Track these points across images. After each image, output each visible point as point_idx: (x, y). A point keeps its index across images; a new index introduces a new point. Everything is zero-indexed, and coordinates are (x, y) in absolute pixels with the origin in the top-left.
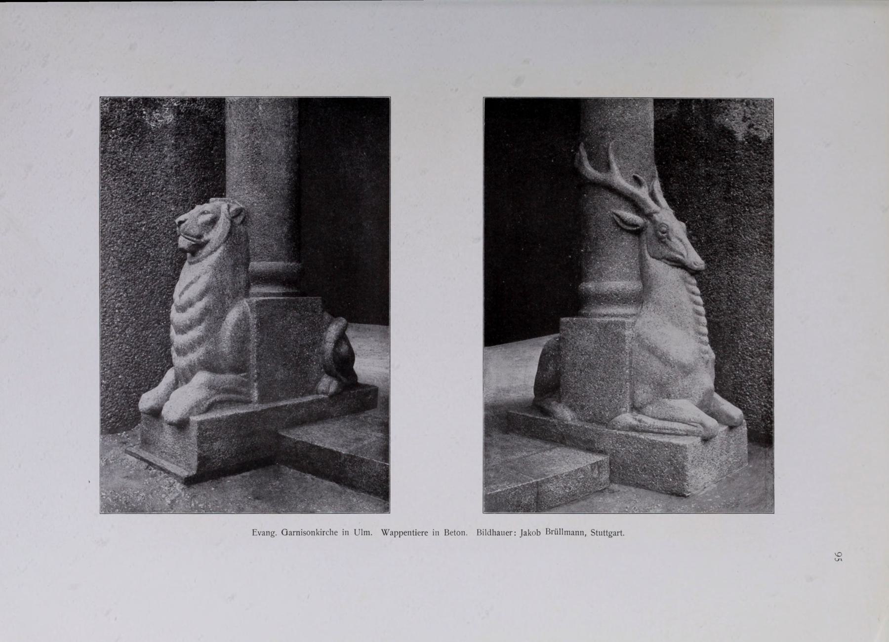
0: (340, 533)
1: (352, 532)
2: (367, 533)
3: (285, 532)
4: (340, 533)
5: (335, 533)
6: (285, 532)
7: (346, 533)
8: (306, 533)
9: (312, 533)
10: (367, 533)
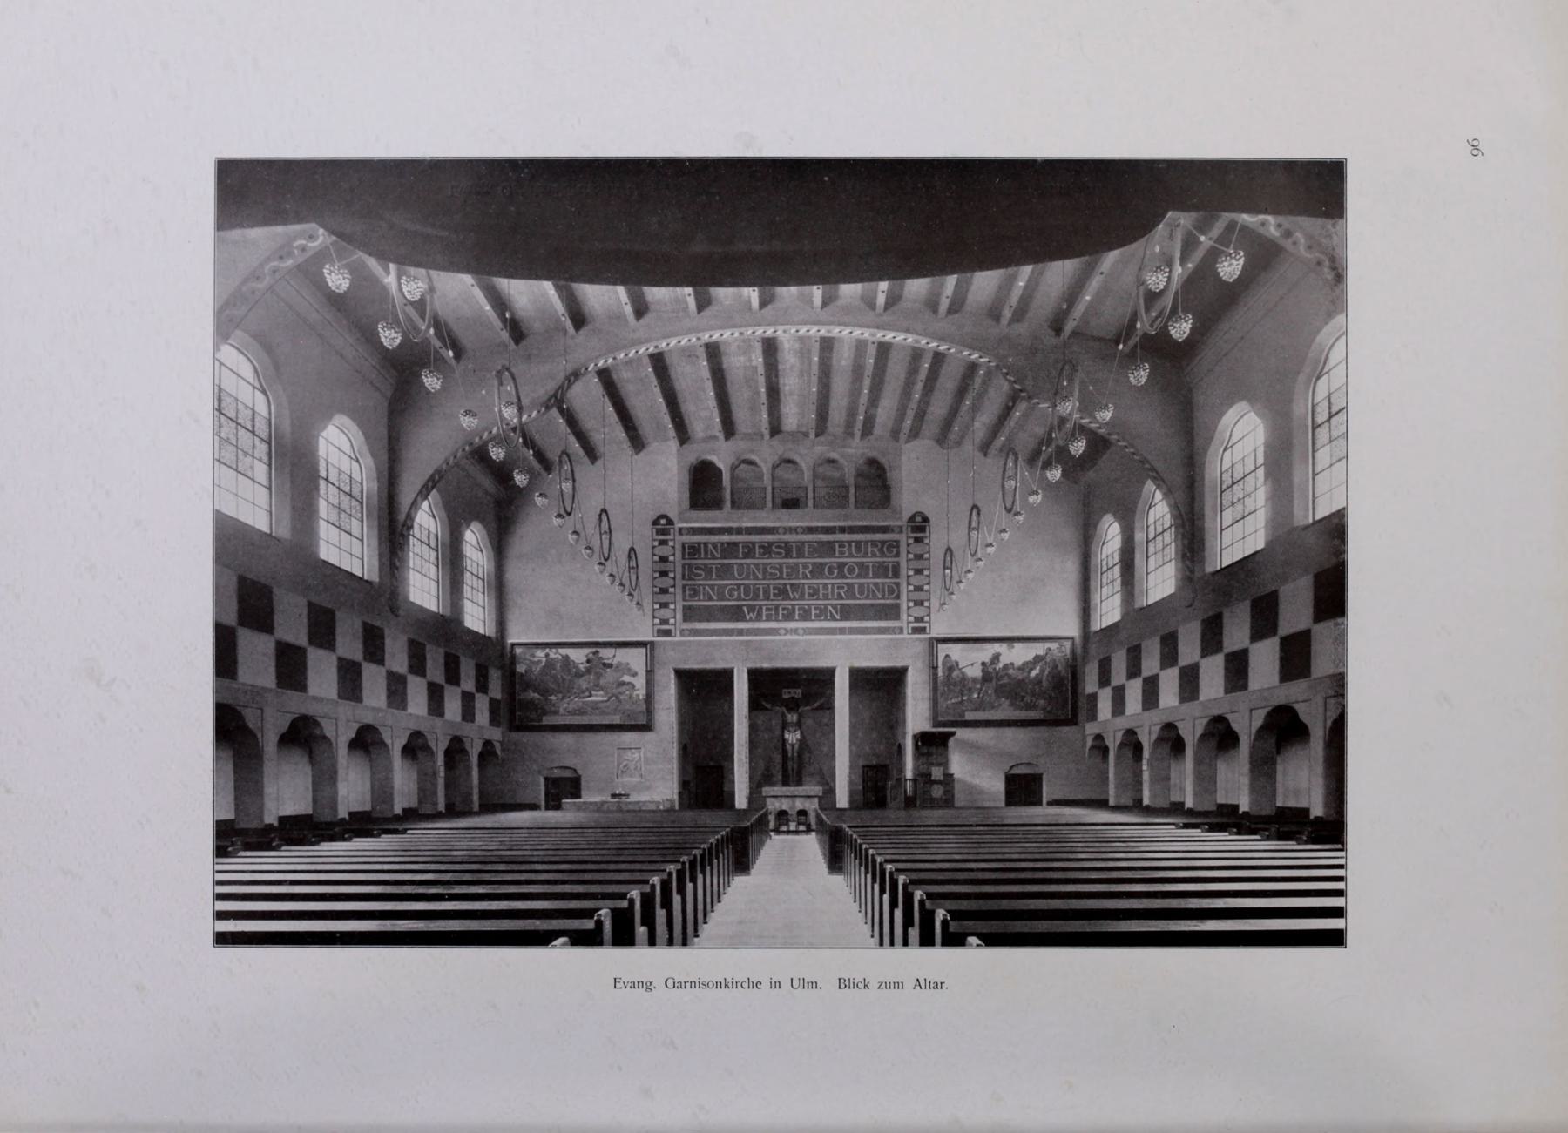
1: (786, 984)
2: (814, 985)
6: (670, 983)
7: (778, 985)
8: (706, 985)
9: (718, 985)
10: (814, 985)
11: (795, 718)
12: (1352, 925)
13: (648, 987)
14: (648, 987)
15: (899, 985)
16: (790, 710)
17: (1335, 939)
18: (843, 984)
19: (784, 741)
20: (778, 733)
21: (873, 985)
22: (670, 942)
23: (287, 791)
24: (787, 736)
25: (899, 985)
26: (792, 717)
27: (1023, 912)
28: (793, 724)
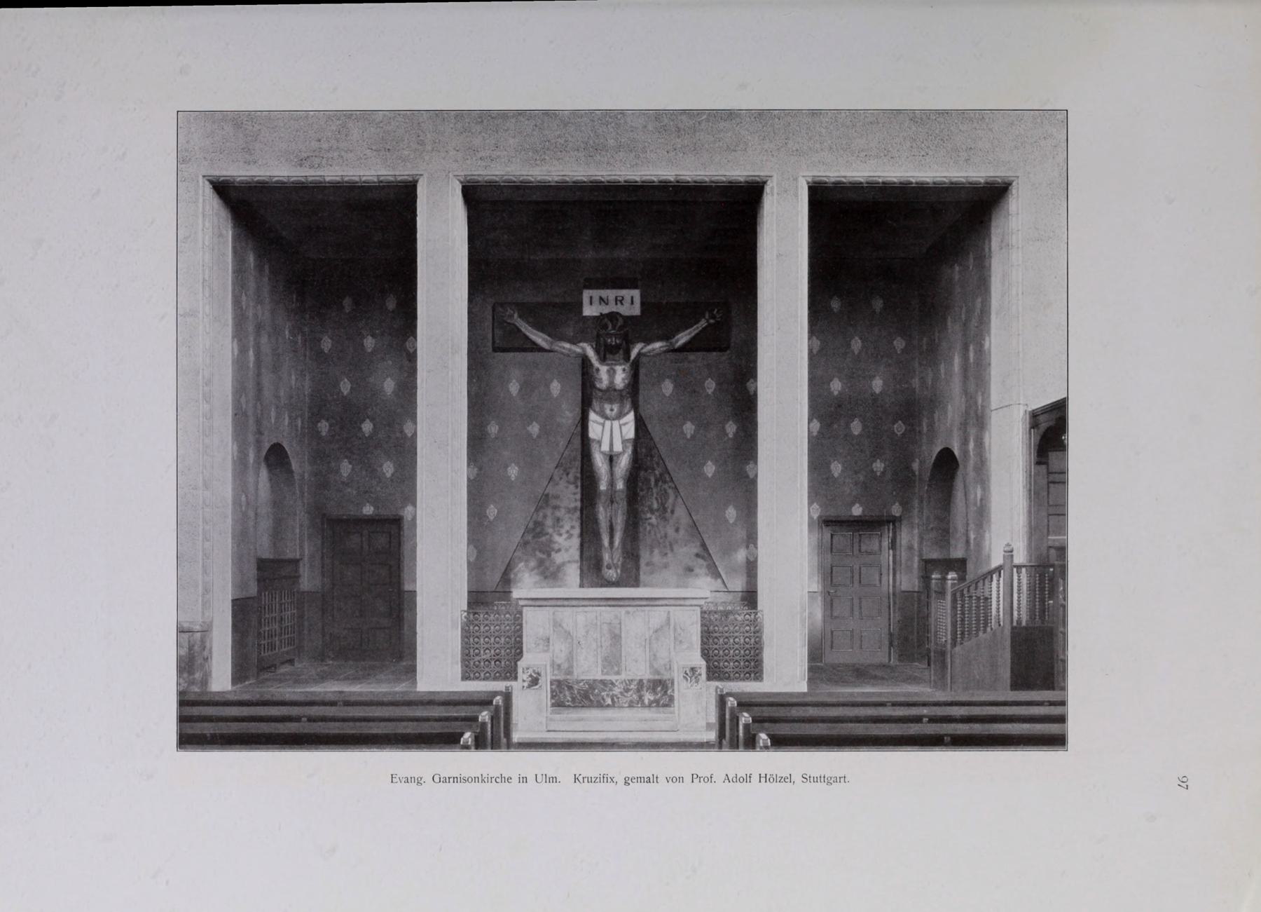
0: (515, 780)
1: (531, 779)
2: (554, 780)
3: (437, 779)
4: (515, 780)
6: (437, 779)
7: (524, 780)
9: (476, 779)
10: (554, 780)
11: (621, 377)
12: (1074, 729)
13: (419, 782)
14: (419, 782)
15: (681, 779)
16: (606, 352)
17: (1058, 741)
19: (585, 443)
20: (568, 415)
21: (797, 778)
22: (1062, 719)
23: (381, 541)
24: (595, 430)
25: (681, 779)
26: (615, 375)
27: (264, 735)
28: (611, 394)
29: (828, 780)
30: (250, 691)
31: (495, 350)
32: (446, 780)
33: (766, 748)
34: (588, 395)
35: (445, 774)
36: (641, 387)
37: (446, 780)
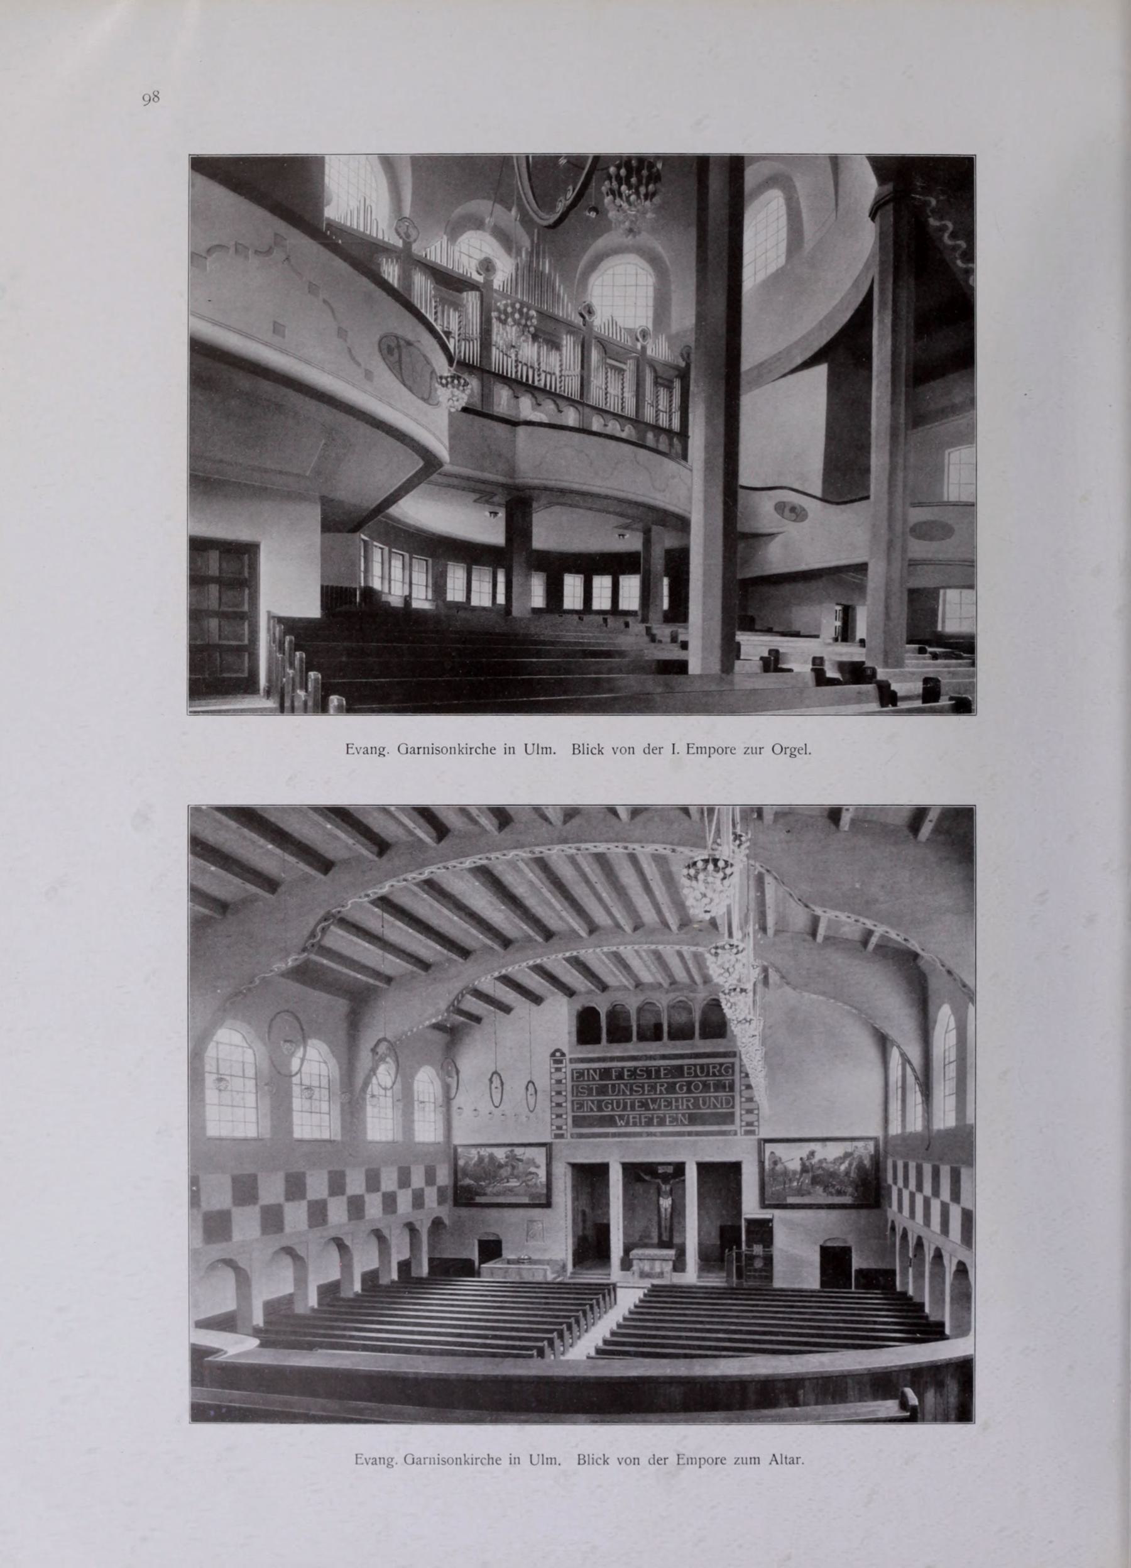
0: (500, 751)
1: (520, 749)
2: (547, 750)
3: (403, 750)
4: (500, 751)
5: (492, 751)
6: (403, 750)
7: (510, 750)
9: (457, 1461)
11: (668, 1188)
18: (577, 749)
21: (391, 748)
26: (666, 1188)
29: (710, 751)
30: (927, 198)
31: (862, 568)
32: (416, 751)
33: (305, 710)
34: (659, 1193)
35: (414, 743)
36: (803, 567)
37: (416, 751)
